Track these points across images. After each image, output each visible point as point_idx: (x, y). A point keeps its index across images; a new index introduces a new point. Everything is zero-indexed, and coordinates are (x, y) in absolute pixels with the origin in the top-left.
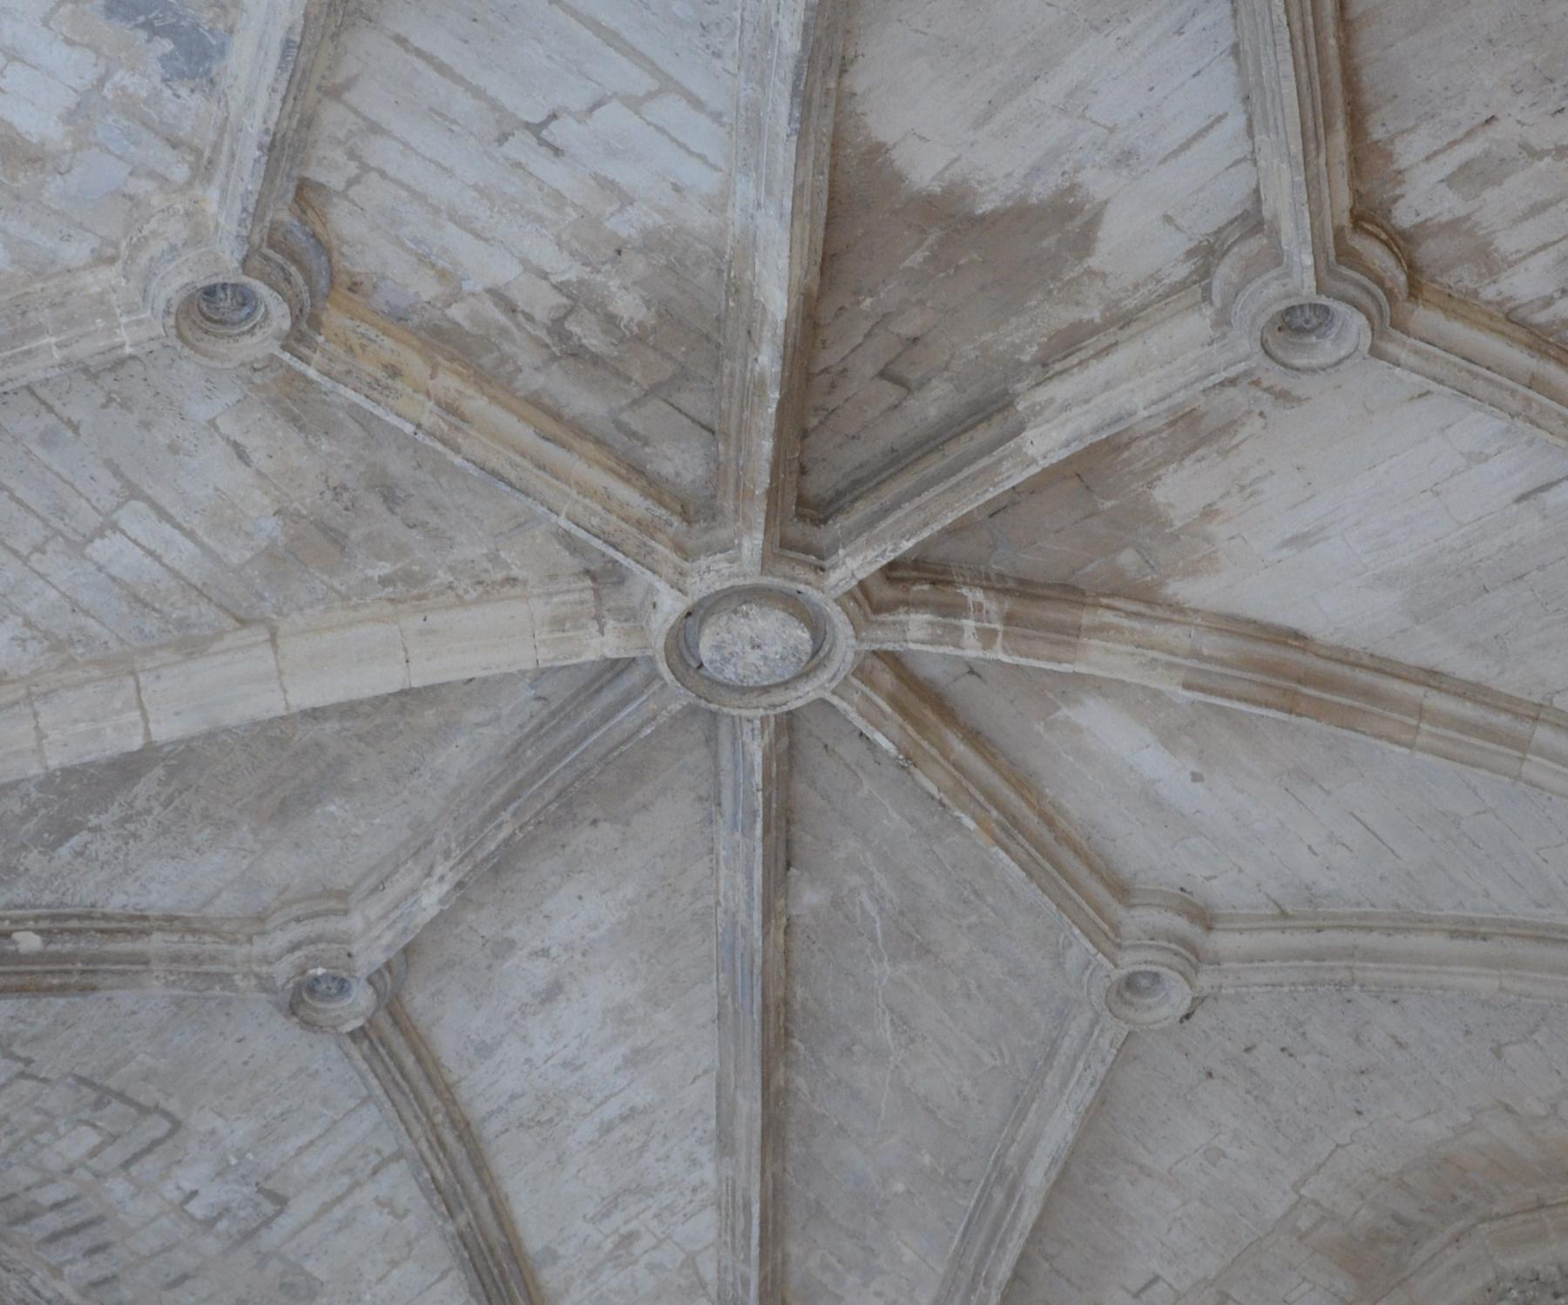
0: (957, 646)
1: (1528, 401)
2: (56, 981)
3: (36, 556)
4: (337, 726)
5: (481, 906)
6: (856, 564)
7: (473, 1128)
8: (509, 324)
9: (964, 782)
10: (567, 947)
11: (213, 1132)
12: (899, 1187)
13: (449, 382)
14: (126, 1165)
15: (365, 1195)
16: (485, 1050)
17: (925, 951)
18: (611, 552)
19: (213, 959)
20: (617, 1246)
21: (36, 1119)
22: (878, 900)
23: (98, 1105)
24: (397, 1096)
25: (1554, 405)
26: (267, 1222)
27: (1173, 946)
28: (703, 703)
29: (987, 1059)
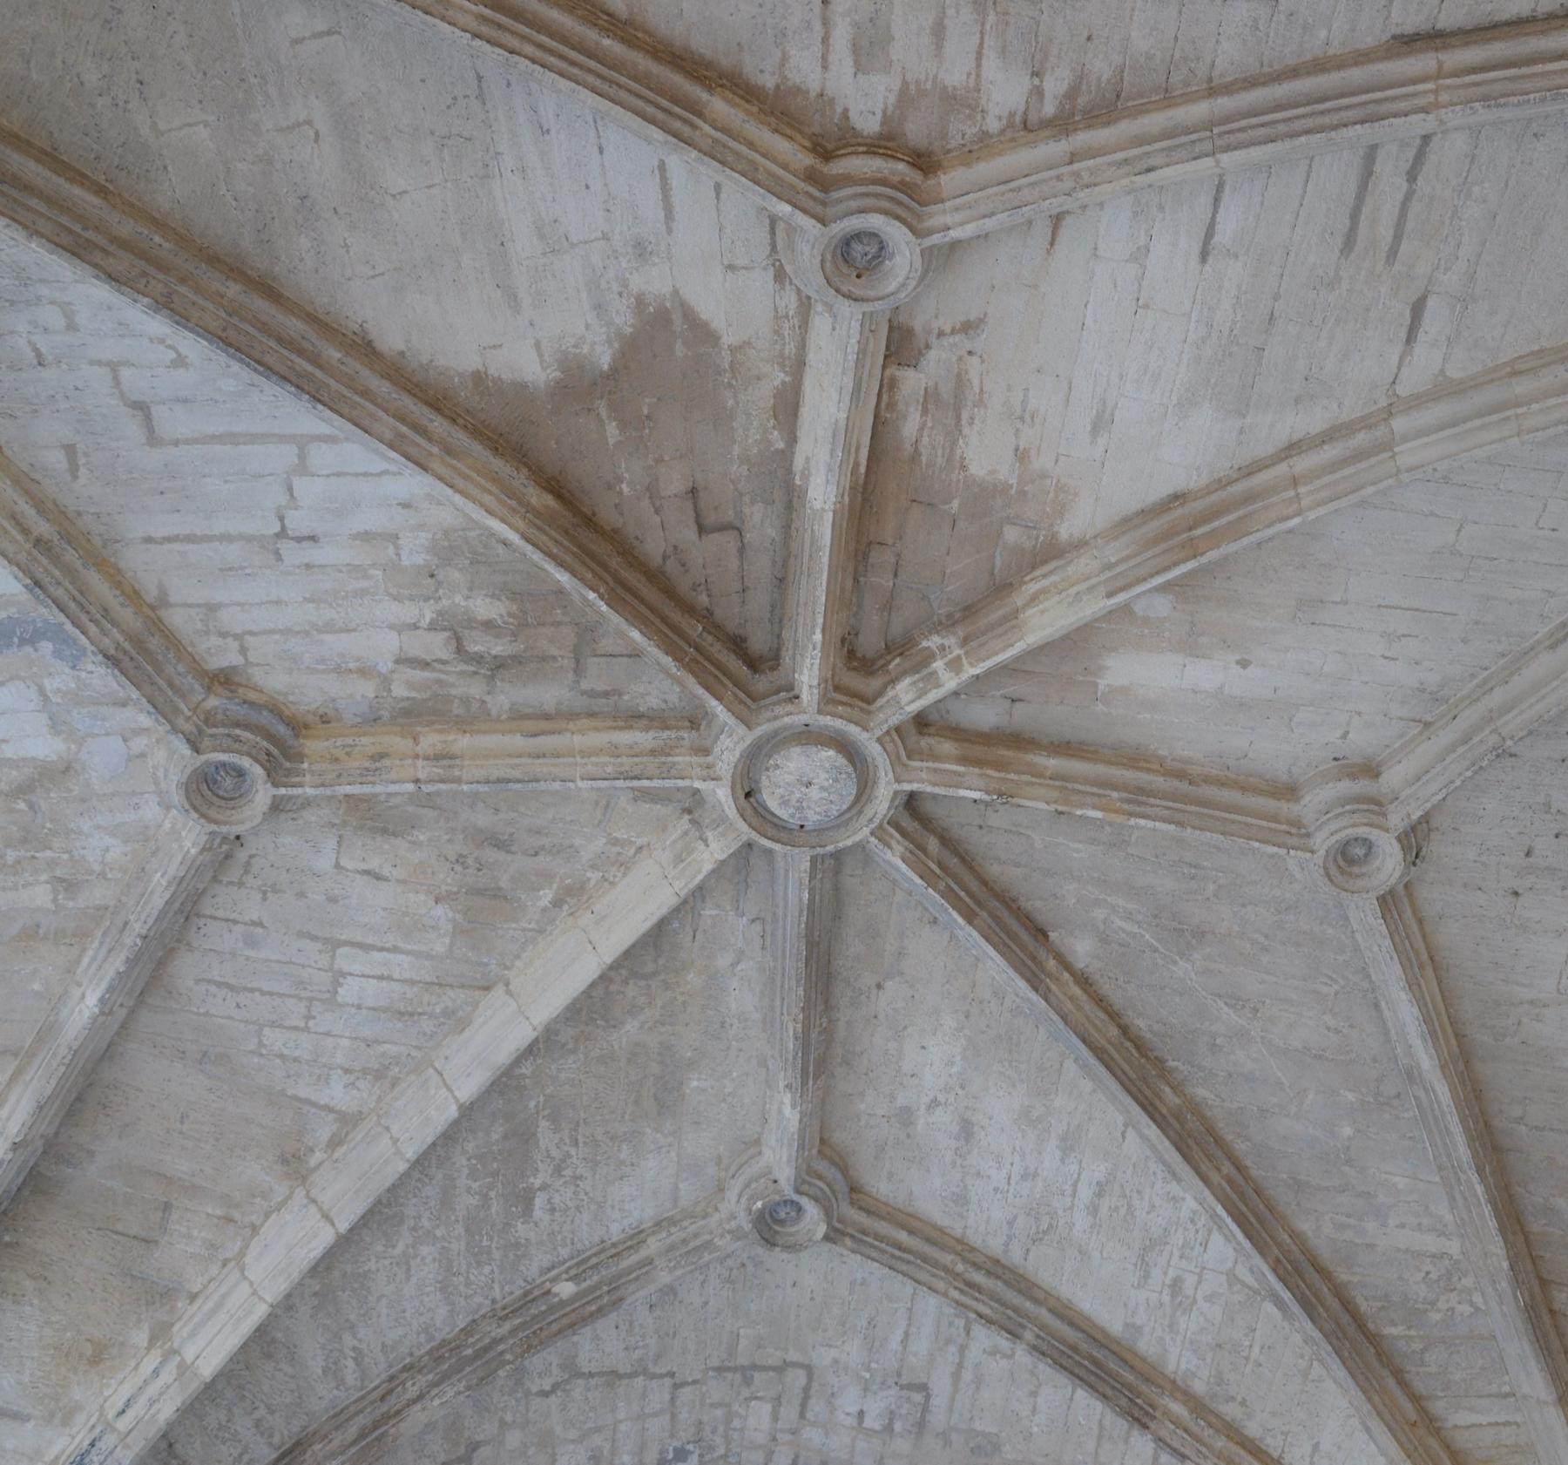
0: (938, 686)
1: (1077, 175)
2: (594, 1308)
3: (311, 1023)
4: (636, 1023)
5: (862, 1094)
6: (809, 671)
7: (1003, 1261)
8: (436, 675)
9: (1070, 786)
10: (947, 1089)
11: (836, 1361)
12: (1348, 1131)
13: (431, 740)
14: (802, 1415)
15: (974, 1353)
16: (961, 1199)
17: (1200, 934)
18: (635, 783)
19: (696, 1235)
20: (1173, 1296)
21: (719, 1413)
22: (1128, 917)
23: (748, 1381)
24: (904, 1267)
25: (1099, 160)
26: (925, 1408)
27: (1348, 807)
28: (819, 850)
29: (1325, 990)
